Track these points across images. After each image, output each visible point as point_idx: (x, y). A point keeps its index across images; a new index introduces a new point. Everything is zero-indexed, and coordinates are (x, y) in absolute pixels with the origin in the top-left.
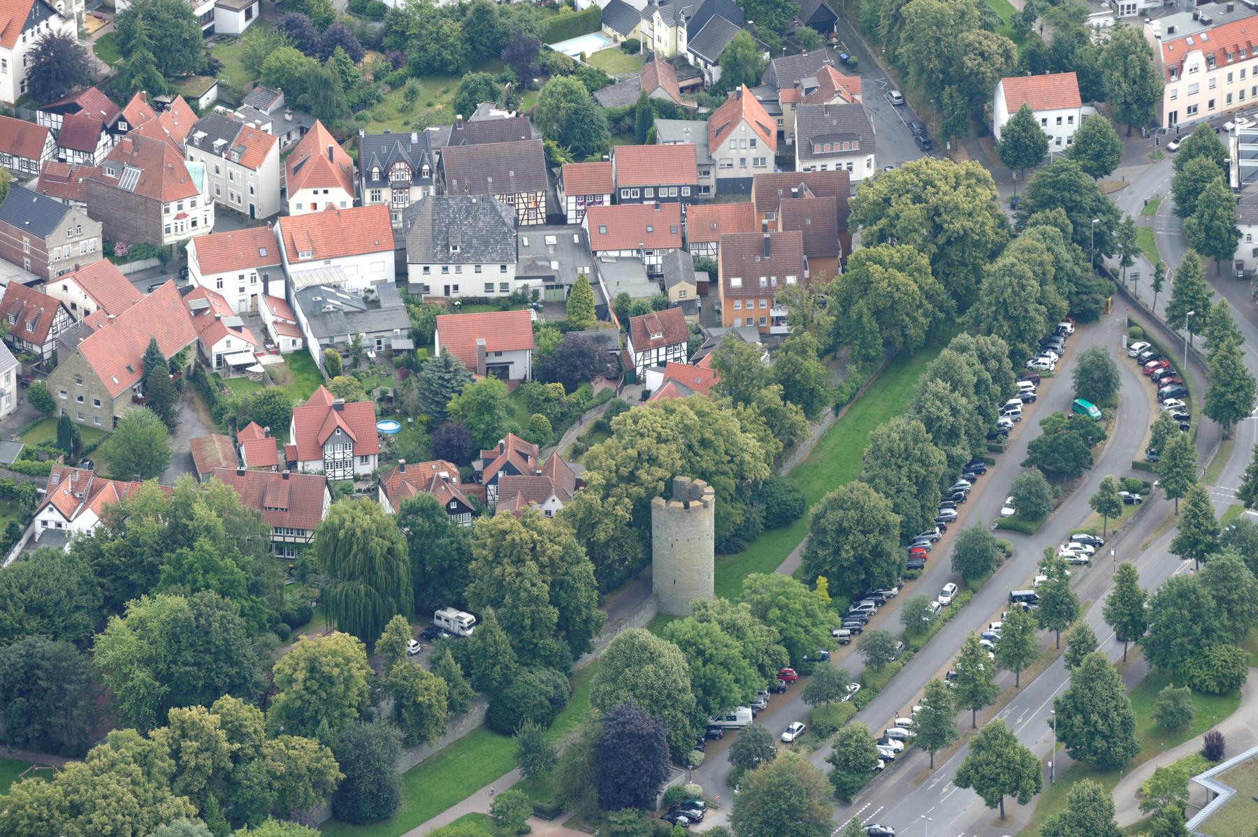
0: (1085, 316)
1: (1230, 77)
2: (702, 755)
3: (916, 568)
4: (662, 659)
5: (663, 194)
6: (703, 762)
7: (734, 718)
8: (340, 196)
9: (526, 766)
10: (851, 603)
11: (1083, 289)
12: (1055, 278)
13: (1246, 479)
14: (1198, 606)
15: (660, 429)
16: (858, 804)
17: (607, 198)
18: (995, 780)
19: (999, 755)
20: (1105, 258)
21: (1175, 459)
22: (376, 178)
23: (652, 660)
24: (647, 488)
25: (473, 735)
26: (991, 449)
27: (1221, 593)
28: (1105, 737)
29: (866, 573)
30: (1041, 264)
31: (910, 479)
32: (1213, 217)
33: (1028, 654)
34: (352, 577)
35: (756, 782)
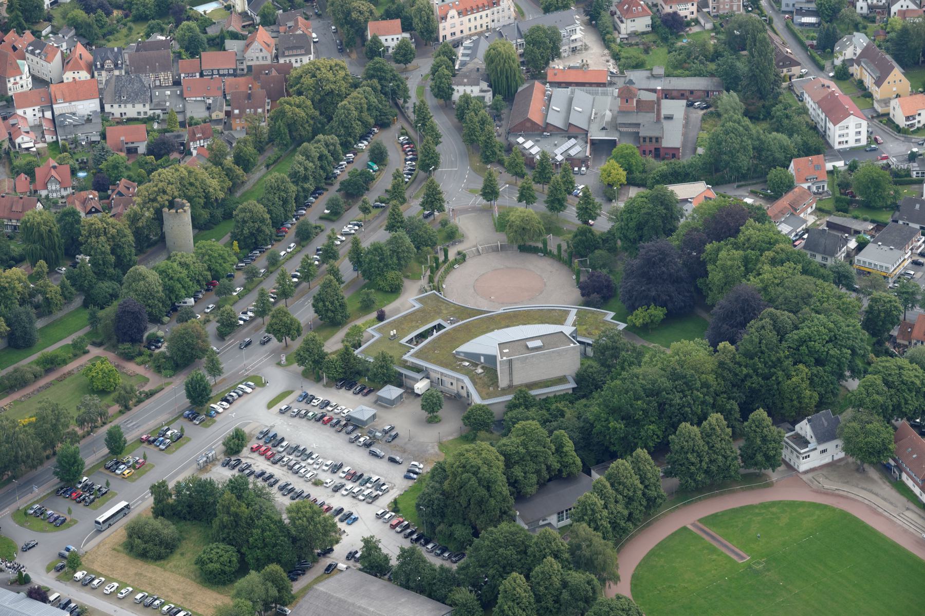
1: (470, 20)
2: (169, 319)
5: (221, 72)
6: (169, 322)
7: (186, 303)
8: (84, 75)
9: (92, 323)
11: (382, 113)
12: (368, 109)
14: (383, 255)
17: (198, 74)
18: (279, 331)
22: (99, 67)
23: (144, 279)
25: (77, 310)
26: (327, 184)
28: (332, 311)
30: (360, 104)
31: (279, 199)
32: (441, 83)
33: (312, 275)
34: (34, 242)
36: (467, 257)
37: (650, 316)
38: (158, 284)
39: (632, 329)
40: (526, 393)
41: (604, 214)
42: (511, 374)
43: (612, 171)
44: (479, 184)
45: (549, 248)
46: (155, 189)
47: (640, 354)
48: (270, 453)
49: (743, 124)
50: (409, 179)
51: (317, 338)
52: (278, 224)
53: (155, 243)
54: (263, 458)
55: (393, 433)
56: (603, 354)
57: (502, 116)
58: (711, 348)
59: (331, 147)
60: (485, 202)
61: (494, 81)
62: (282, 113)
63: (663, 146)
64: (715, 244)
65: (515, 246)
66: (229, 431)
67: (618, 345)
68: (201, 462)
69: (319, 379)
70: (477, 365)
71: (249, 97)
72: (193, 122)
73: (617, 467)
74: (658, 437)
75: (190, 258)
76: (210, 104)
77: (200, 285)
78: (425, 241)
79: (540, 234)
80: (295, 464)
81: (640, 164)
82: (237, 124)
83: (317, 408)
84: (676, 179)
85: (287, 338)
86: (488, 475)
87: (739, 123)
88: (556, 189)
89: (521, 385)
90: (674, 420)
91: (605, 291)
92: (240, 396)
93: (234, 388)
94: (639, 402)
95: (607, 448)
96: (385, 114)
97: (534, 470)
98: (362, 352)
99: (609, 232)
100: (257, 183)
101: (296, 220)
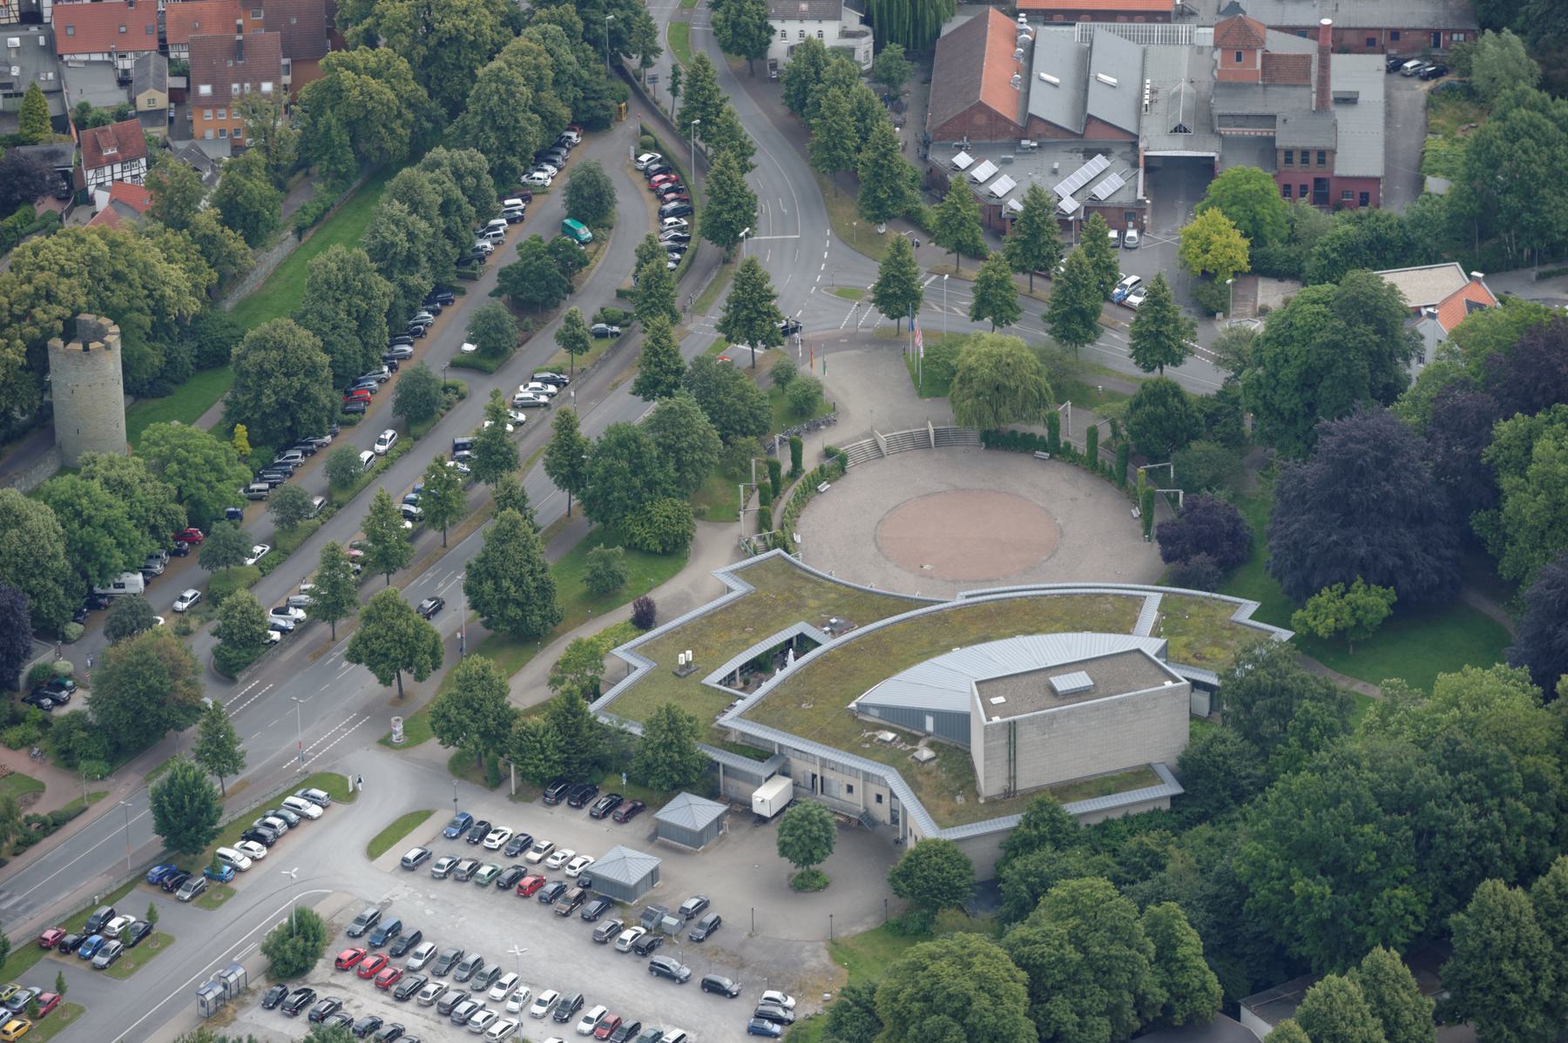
0: (594, 124)
2: (81, 628)
3: (355, 412)
4: (28, 523)
6: (82, 636)
7: (122, 586)
10: (278, 452)
11: (591, 94)
12: (556, 82)
13: (727, 310)
14: (640, 455)
15: (63, 262)
16: (244, 682)
18: (386, 655)
19: (391, 628)
20: (624, 58)
21: (649, 288)
23: (18, 524)
24: (42, 328)
26: (461, 277)
27: (668, 441)
28: (518, 604)
29: (293, 419)
30: (537, 68)
31: (349, 314)
32: (740, 12)
33: (452, 510)
35: (112, 661)
36: (850, 463)
37: (1354, 610)
38: (54, 536)
39: (1308, 643)
40: (1056, 810)
41: (1203, 354)
42: (1012, 760)
43: (1215, 237)
44: (868, 277)
45: (1063, 439)
46: (26, 288)
47: (1345, 705)
48: (387, 972)
49: (1555, 112)
50: (677, 262)
51: (493, 672)
52: (347, 379)
53: (24, 431)
54: (370, 984)
55: (709, 918)
56: (1248, 707)
57: (904, 100)
58: (1537, 690)
59: (470, 181)
60: (882, 319)
61: (880, 8)
62: (335, 93)
63: (1337, 173)
64: (1521, 420)
65: (974, 433)
66: (278, 917)
67: (1288, 682)
68: (209, 997)
69: (495, 781)
70: (916, 739)
71: (238, 50)
72: (89, 118)
73: (1328, 995)
74: (1417, 918)
75: (133, 469)
76: (126, 72)
77: (159, 539)
78: (740, 421)
79: (1041, 402)
80: (457, 1001)
81: (1283, 220)
82: (207, 124)
83: (498, 855)
84: (1383, 259)
85: (403, 673)
86: (993, 1019)
87: (1542, 111)
88: (1075, 285)
89: (1039, 790)
90: (1459, 874)
91: (1226, 546)
92: (291, 826)
93: (275, 805)
94: (1368, 828)
95: (1281, 948)
96: (598, 95)
97: (1103, 1008)
98: (608, 708)
99: (1221, 395)
100: (275, 274)
101: (391, 369)
